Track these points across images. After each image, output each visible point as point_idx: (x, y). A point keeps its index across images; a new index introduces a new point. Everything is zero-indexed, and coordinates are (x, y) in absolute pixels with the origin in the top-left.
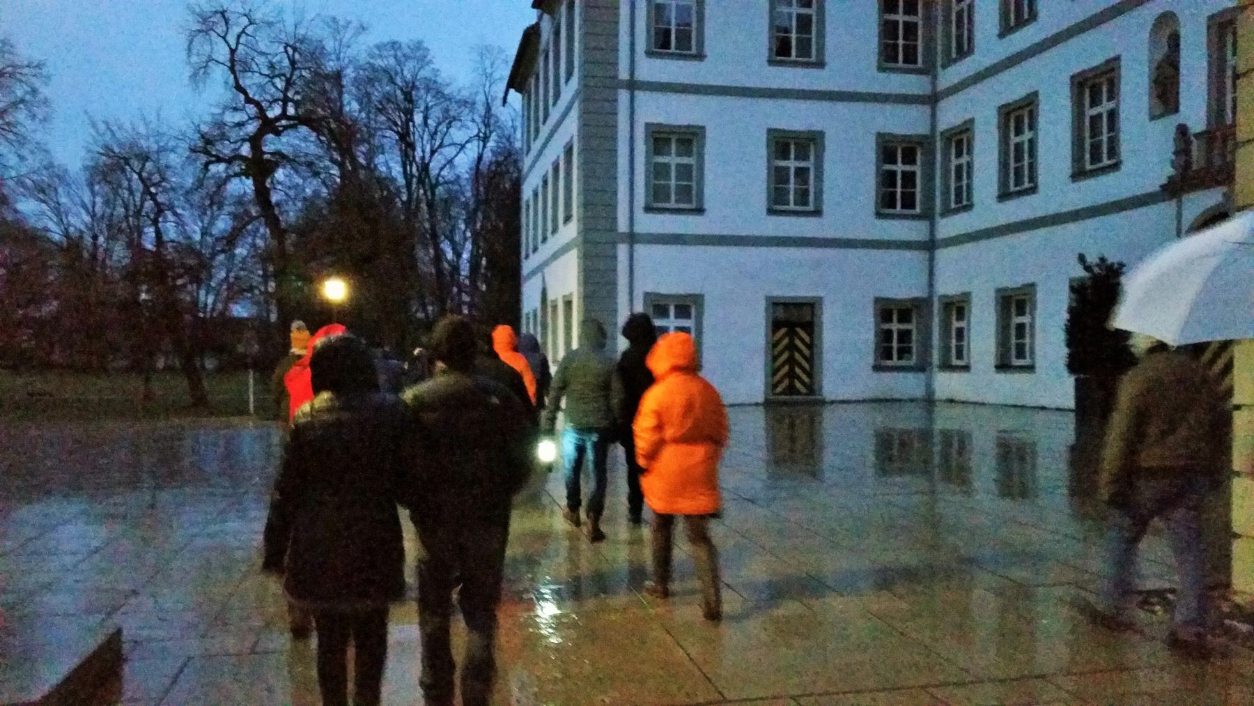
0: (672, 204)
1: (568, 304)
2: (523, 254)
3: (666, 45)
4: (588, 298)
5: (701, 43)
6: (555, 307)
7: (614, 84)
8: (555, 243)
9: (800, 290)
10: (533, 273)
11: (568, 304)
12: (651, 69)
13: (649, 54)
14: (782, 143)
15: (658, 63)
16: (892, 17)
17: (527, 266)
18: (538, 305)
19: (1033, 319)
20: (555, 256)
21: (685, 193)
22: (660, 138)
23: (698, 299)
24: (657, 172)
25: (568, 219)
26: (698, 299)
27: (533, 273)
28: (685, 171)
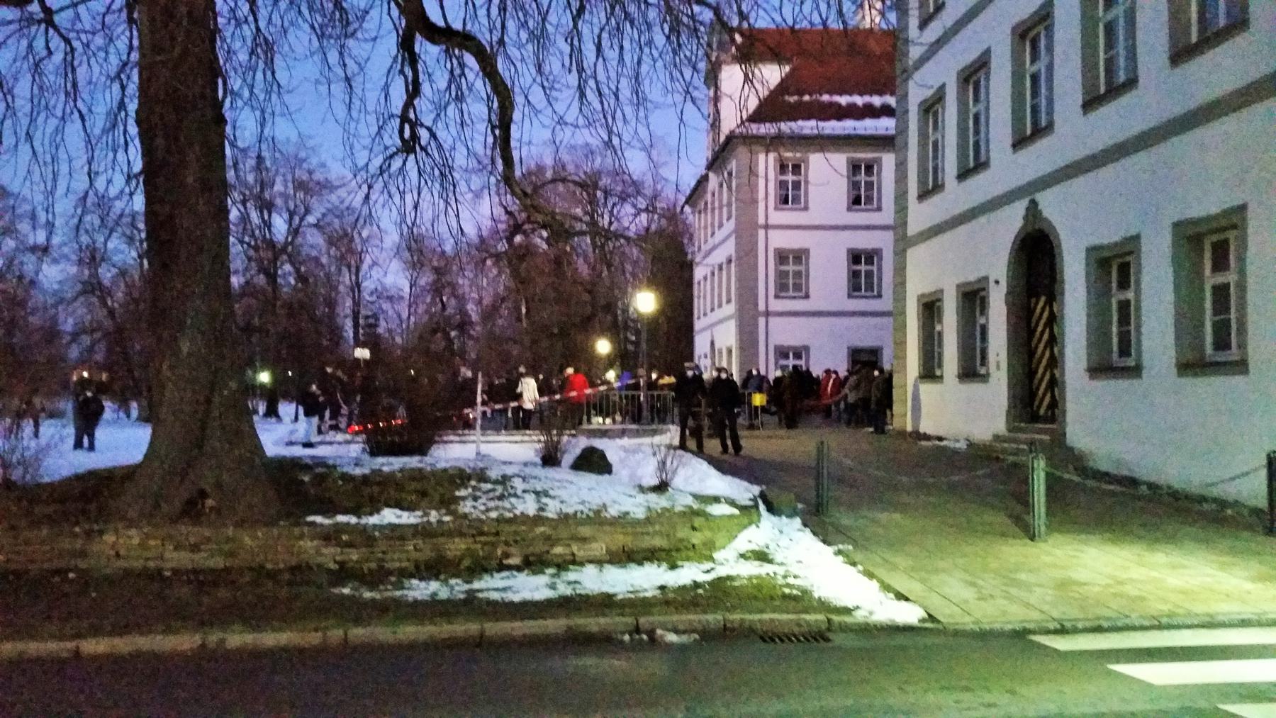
0: (791, 293)
1: (730, 351)
2: (696, 316)
3: (786, 202)
4: (742, 349)
5: (806, 202)
6: (720, 352)
7: (756, 226)
8: (720, 235)
9: (867, 342)
10: (704, 329)
11: (730, 351)
12: (778, 217)
13: (776, 208)
14: (855, 257)
15: (779, 214)
16: (858, 268)
17: (698, 325)
18: (708, 350)
19: (1242, 273)
20: (721, 321)
21: (797, 287)
22: (782, 256)
23: (807, 348)
24: (782, 276)
25: (728, 219)
26: (807, 348)
27: (704, 329)
28: (798, 274)
